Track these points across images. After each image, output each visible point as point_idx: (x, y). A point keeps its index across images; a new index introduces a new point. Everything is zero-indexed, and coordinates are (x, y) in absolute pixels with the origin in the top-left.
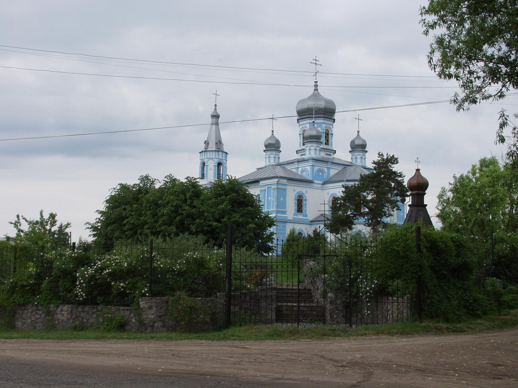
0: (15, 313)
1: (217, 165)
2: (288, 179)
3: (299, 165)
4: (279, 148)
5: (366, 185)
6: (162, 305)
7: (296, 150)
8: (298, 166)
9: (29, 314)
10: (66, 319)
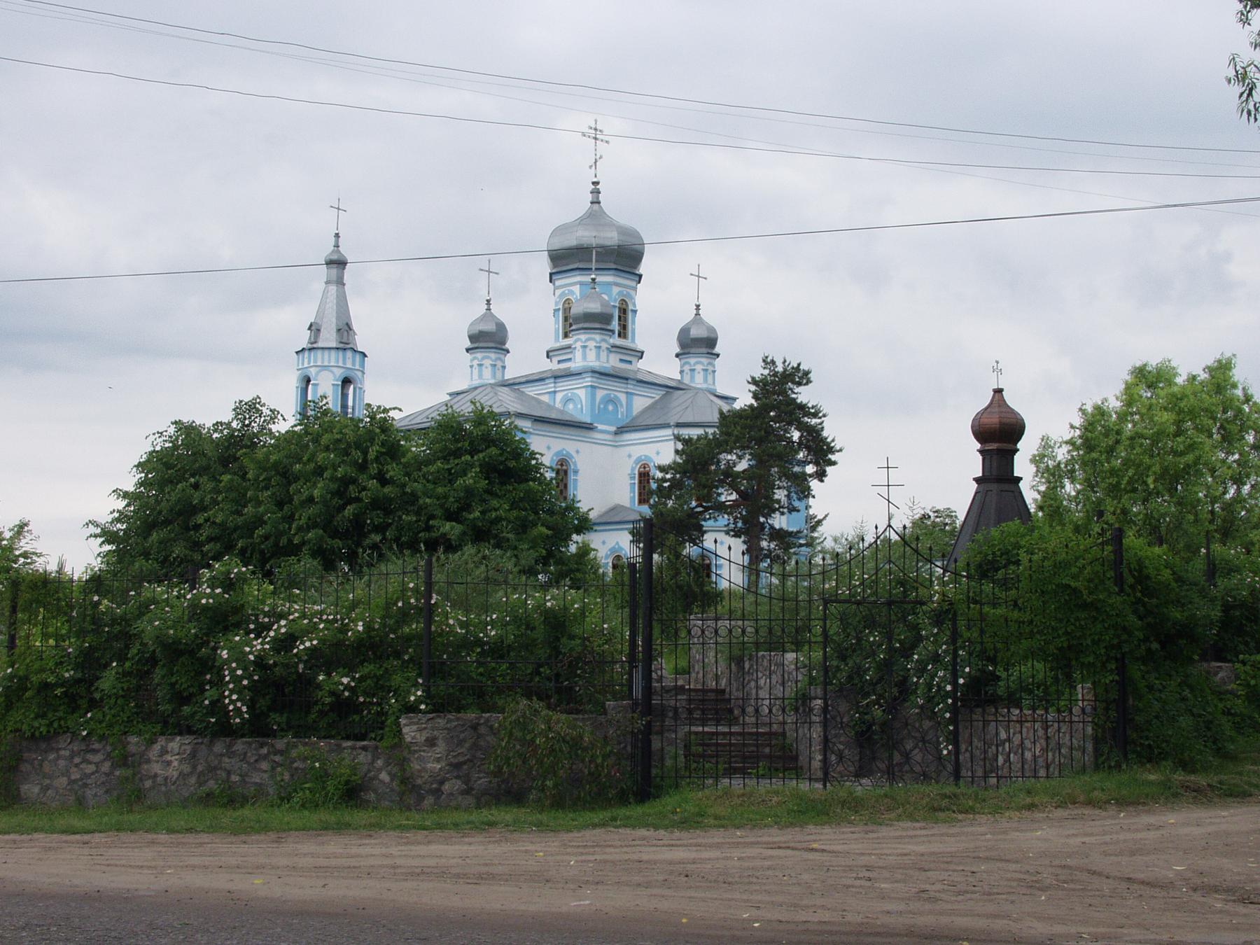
0: (20, 760)
1: (340, 383)
2: (535, 420)
3: (558, 385)
4: (505, 344)
5: (737, 436)
6: (462, 736)
7: (548, 348)
8: (555, 387)
9: (62, 763)
10: (176, 774)
